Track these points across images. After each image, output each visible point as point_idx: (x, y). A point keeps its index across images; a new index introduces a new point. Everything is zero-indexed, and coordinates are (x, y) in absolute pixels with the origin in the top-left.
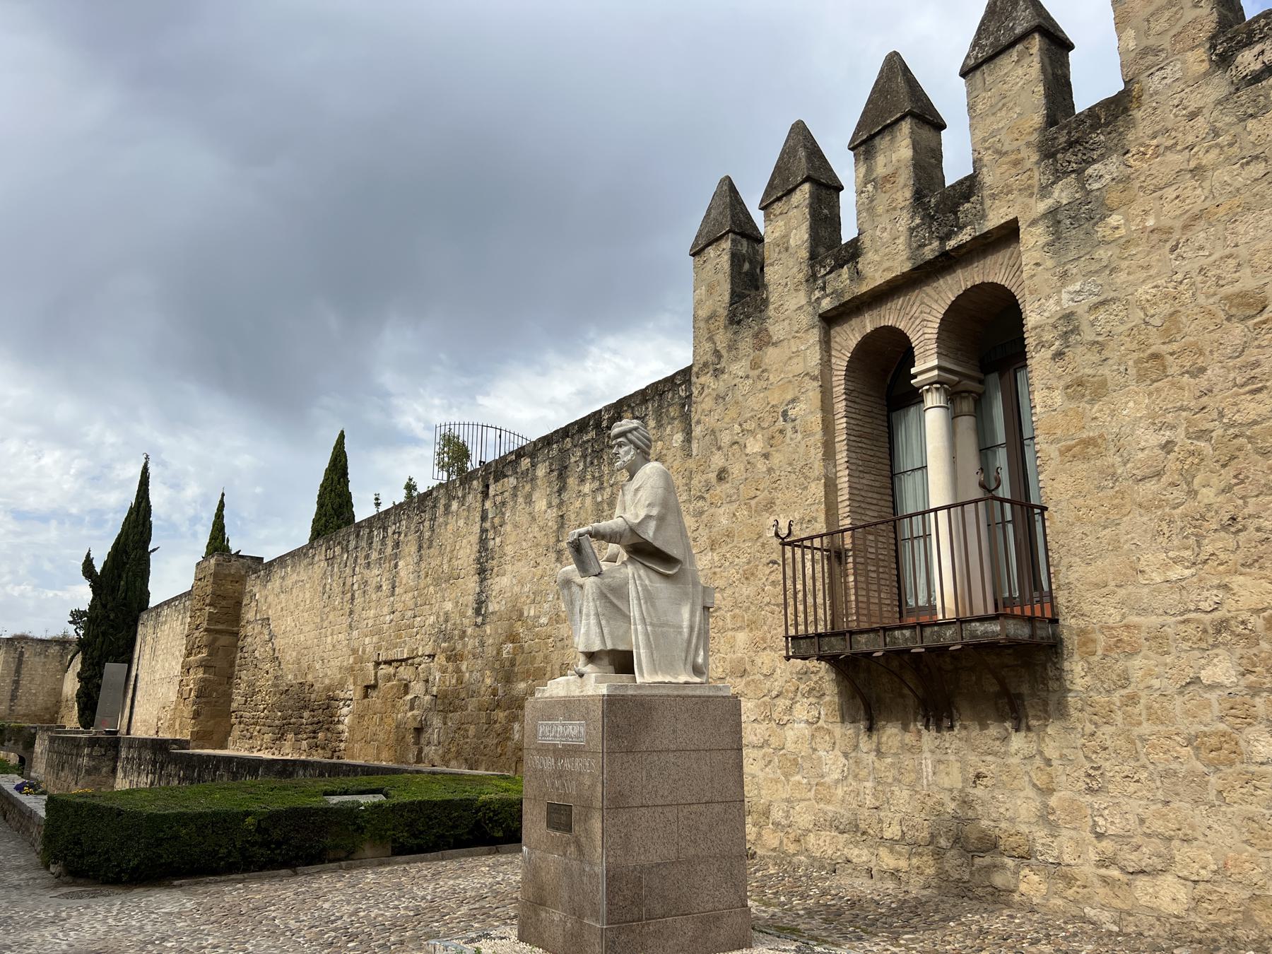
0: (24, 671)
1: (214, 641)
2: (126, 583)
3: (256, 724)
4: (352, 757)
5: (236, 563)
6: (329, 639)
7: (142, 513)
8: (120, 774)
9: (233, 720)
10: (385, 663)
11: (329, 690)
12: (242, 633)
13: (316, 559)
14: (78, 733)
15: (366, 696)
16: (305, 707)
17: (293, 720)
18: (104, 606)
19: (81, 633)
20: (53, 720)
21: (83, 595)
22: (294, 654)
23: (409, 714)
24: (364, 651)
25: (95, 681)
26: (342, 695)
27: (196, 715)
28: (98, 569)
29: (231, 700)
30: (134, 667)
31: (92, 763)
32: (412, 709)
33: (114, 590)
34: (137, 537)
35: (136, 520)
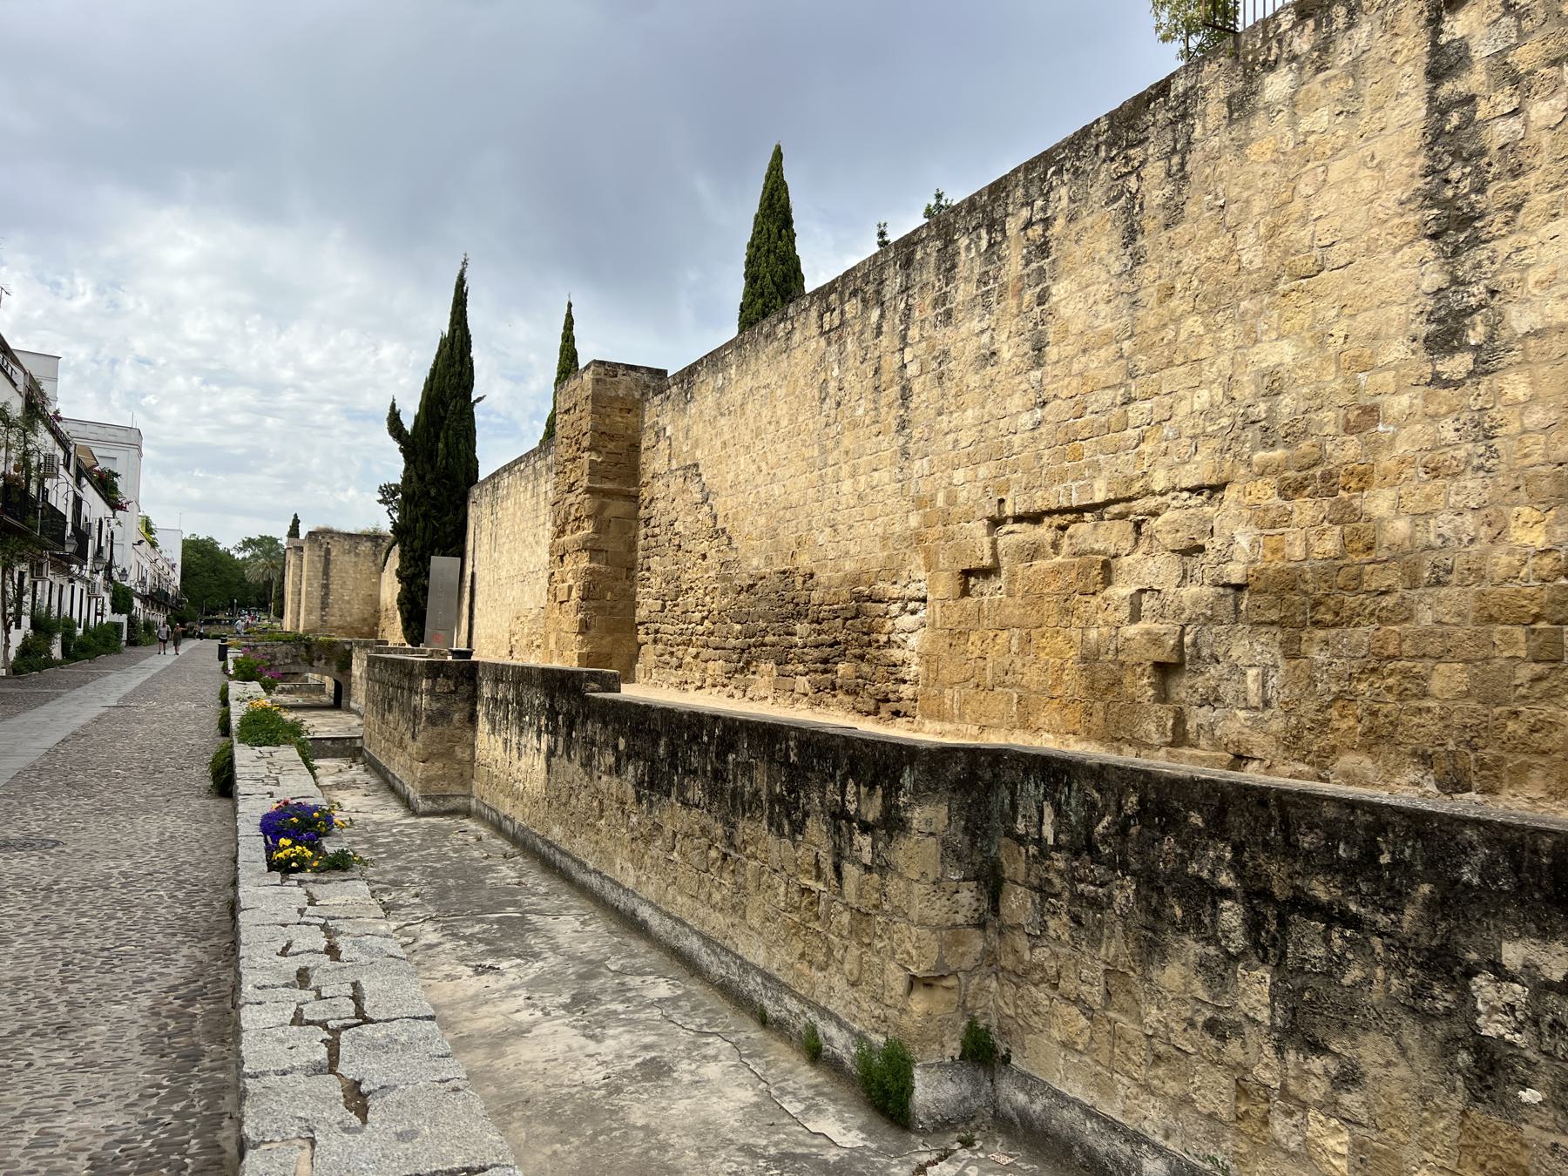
0: (333, 572)
1: (602, 508)
2: (446, 445)
3: (688, 643)
4: (883, 705)
5: (625, 381)
6: (846, 486)
7: (457, 345)
8: (483, 725)
9: (641, 637)
10: (1018, 519)
11: (857, 581)
12: (645, 494)
13: (797, 337)
14: (405, 651)
15: (965, 592)
16: (798, 616)
17: (769, 639)
18: (421, 478)
19: (396, 515)
20: (374, 634)
21: (393, 466)
22: (762, 521)
23: (1131, 630)
24: (951, 500)
25: (420, 581)
26: (894, 591)
27: (584, 627)
28: (408, 425)
29: (634, 606)
30: (469, 563)
31: (436, 706)
32: (1135, 616)
33: (432, 455)
34: (454, 381)
35: (451, 356)
